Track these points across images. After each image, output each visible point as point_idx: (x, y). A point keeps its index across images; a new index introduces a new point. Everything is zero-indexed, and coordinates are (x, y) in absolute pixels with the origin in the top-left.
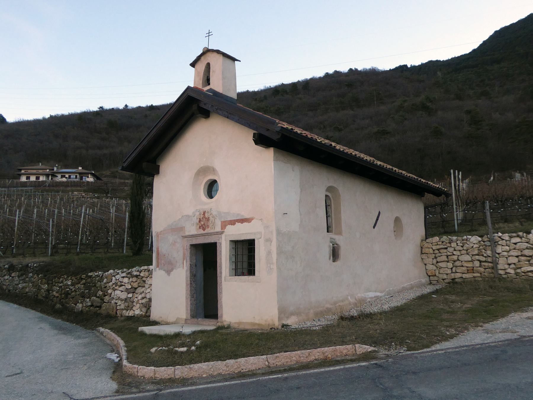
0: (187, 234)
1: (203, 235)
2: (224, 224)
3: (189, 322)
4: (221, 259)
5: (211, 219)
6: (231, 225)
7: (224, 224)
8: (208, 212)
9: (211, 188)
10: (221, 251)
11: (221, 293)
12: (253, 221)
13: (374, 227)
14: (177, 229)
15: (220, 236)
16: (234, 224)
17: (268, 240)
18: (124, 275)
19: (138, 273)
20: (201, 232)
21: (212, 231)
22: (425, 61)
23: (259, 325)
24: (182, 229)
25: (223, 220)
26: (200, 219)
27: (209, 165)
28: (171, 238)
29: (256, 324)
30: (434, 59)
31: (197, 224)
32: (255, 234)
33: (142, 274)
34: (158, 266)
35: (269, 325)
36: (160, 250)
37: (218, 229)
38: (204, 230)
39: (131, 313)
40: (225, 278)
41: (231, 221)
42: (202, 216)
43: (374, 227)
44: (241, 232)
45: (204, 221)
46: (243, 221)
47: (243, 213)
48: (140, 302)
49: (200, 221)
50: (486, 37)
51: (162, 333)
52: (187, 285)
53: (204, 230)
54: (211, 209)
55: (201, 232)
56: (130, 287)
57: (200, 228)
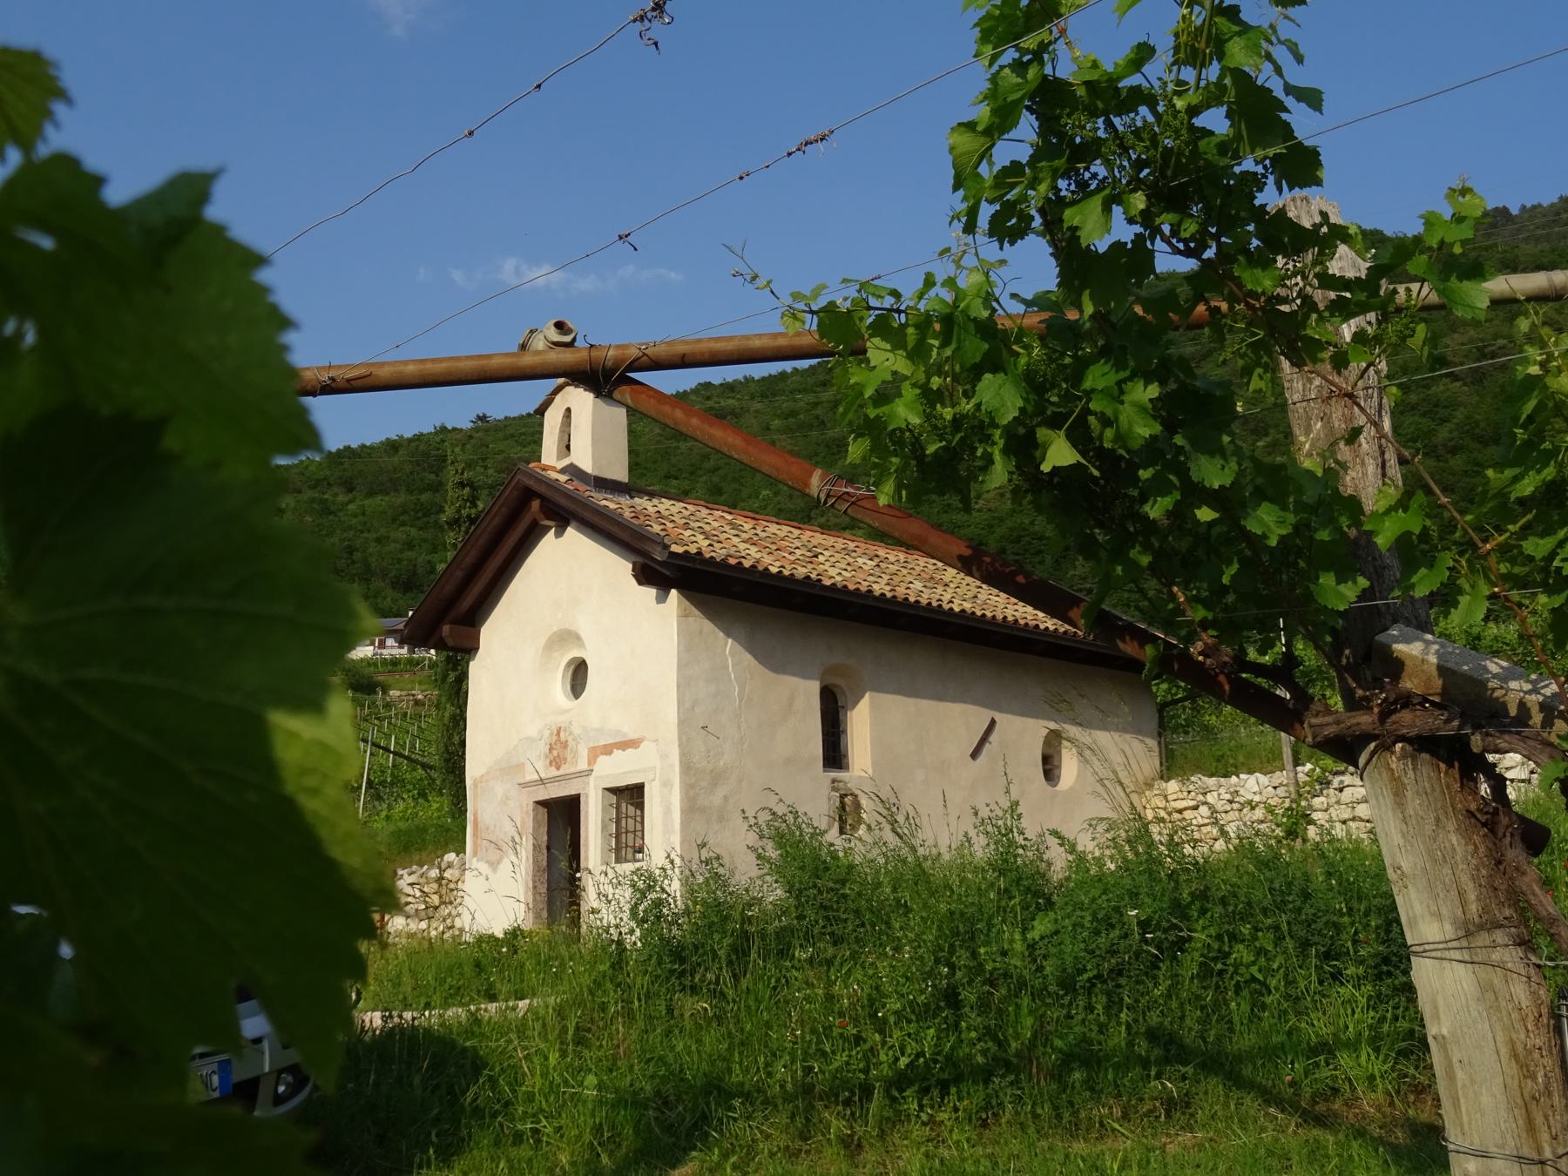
5: (571, 743)
9: (578, 674)
13: (975, 755)
16: (610, 753)
17: (666, 784)
20: (554, 772)
34: (475, 854)
37: (582, 765)
41: (605, 746)
43: (975, 755)
44: (620, 769)
47: (625, 729)
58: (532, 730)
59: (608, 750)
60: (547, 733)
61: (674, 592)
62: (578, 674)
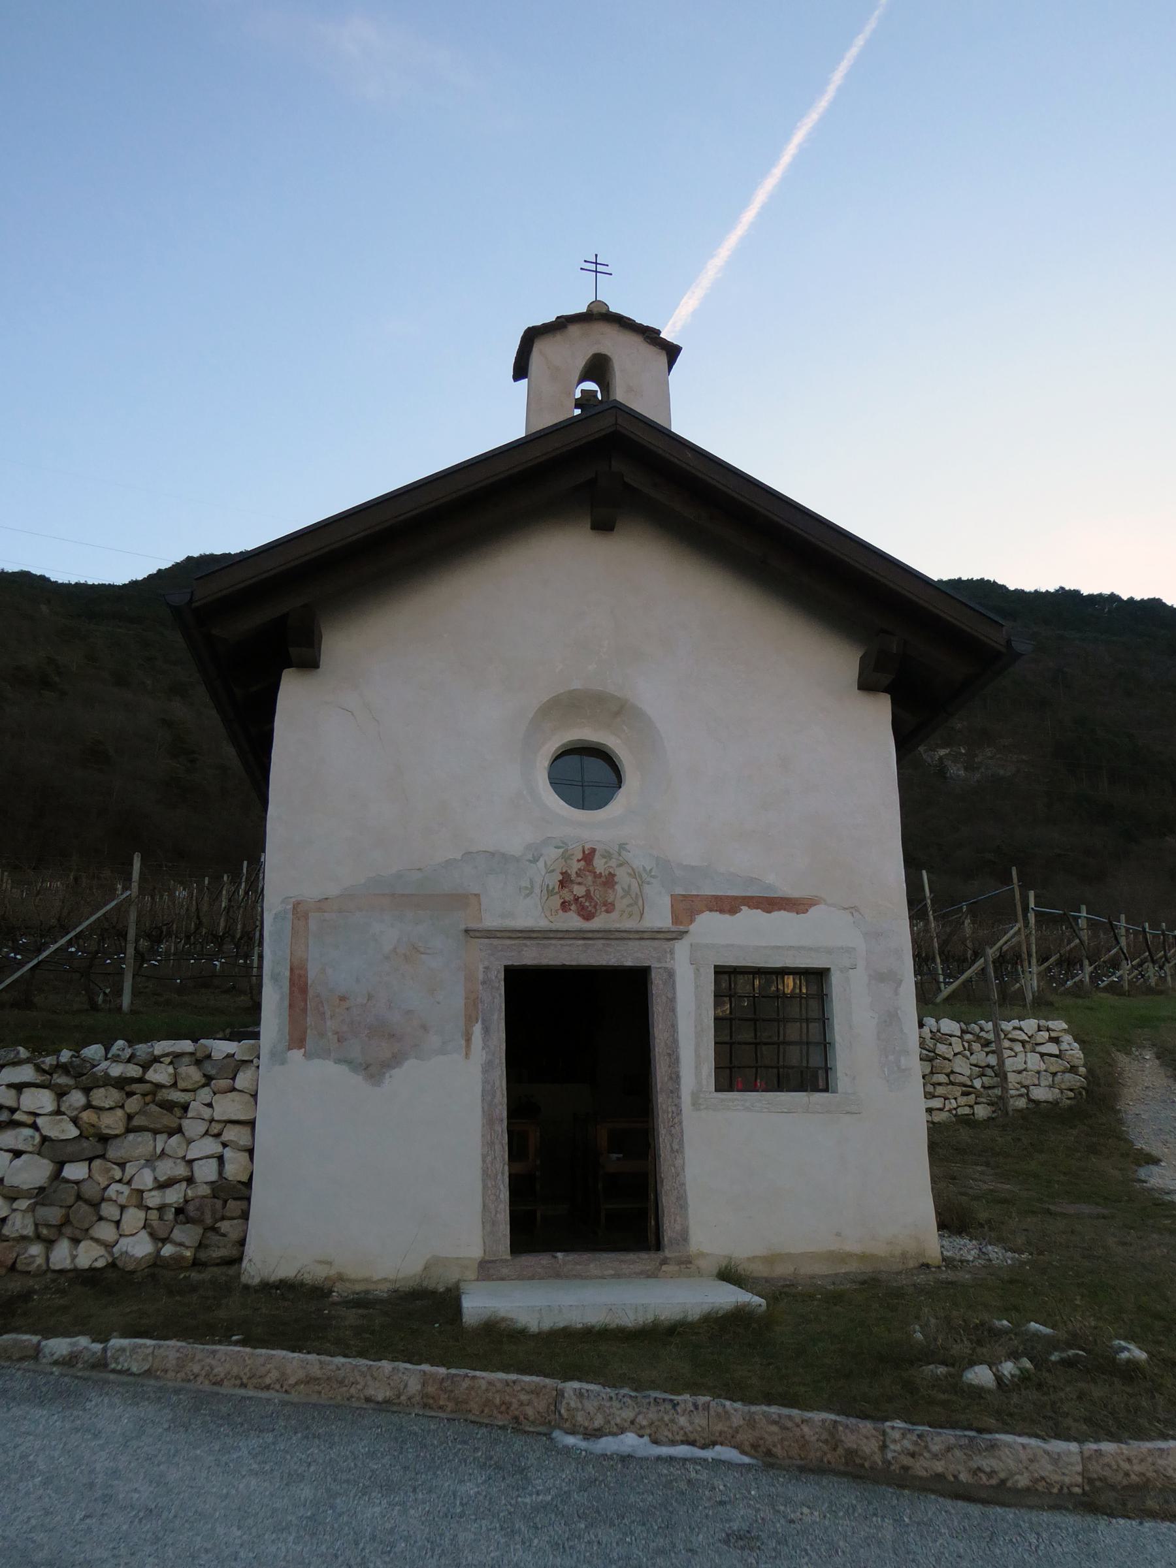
0: (490, 922)
1: (581, 935)
3: (505, 1271)
4: (673, 1027)
5: (622, 875)
6: (721, 911)
7: (687, 908)
8: (607, 855)
9: (588, 772)
12: (812, 910)
15: (667, 945)
16: (733, 911)
17: (883, 977)
18: (26, 1073)
19: (134, 1071)
20: (573, 921)
21: (629, 924)
22: (976, 577)
23: (863, 1257)
24: (461, 900)
25: (680, 891)
26: (565, 874)
29: (850, 1255)
30: (1000, 582)
31: (551, 893)
32: (829, 951)
33: (151, 1075)
34: (297, 1039)
35: (904, 1255)
36: (312, 975)
37: (659, 917)
39: (88, 1256)
40: (695, 1097)
41: (716, 898)
42: (575, 866)
45: (585, 883)
46: (770, 904)
47: (771, 879)
48: (153, 1199)
49: (562, 884)
50: (166, 565)
51: (629, 1319)
52: (489, 1121)
53: (588, 917)
54: (622, 846)
55: (573, 921)
56: (73, 1132)
57: (565, 906)
58: (515, 841)
59: (728, 905)
60: (552, 853)
62: (588, 772)
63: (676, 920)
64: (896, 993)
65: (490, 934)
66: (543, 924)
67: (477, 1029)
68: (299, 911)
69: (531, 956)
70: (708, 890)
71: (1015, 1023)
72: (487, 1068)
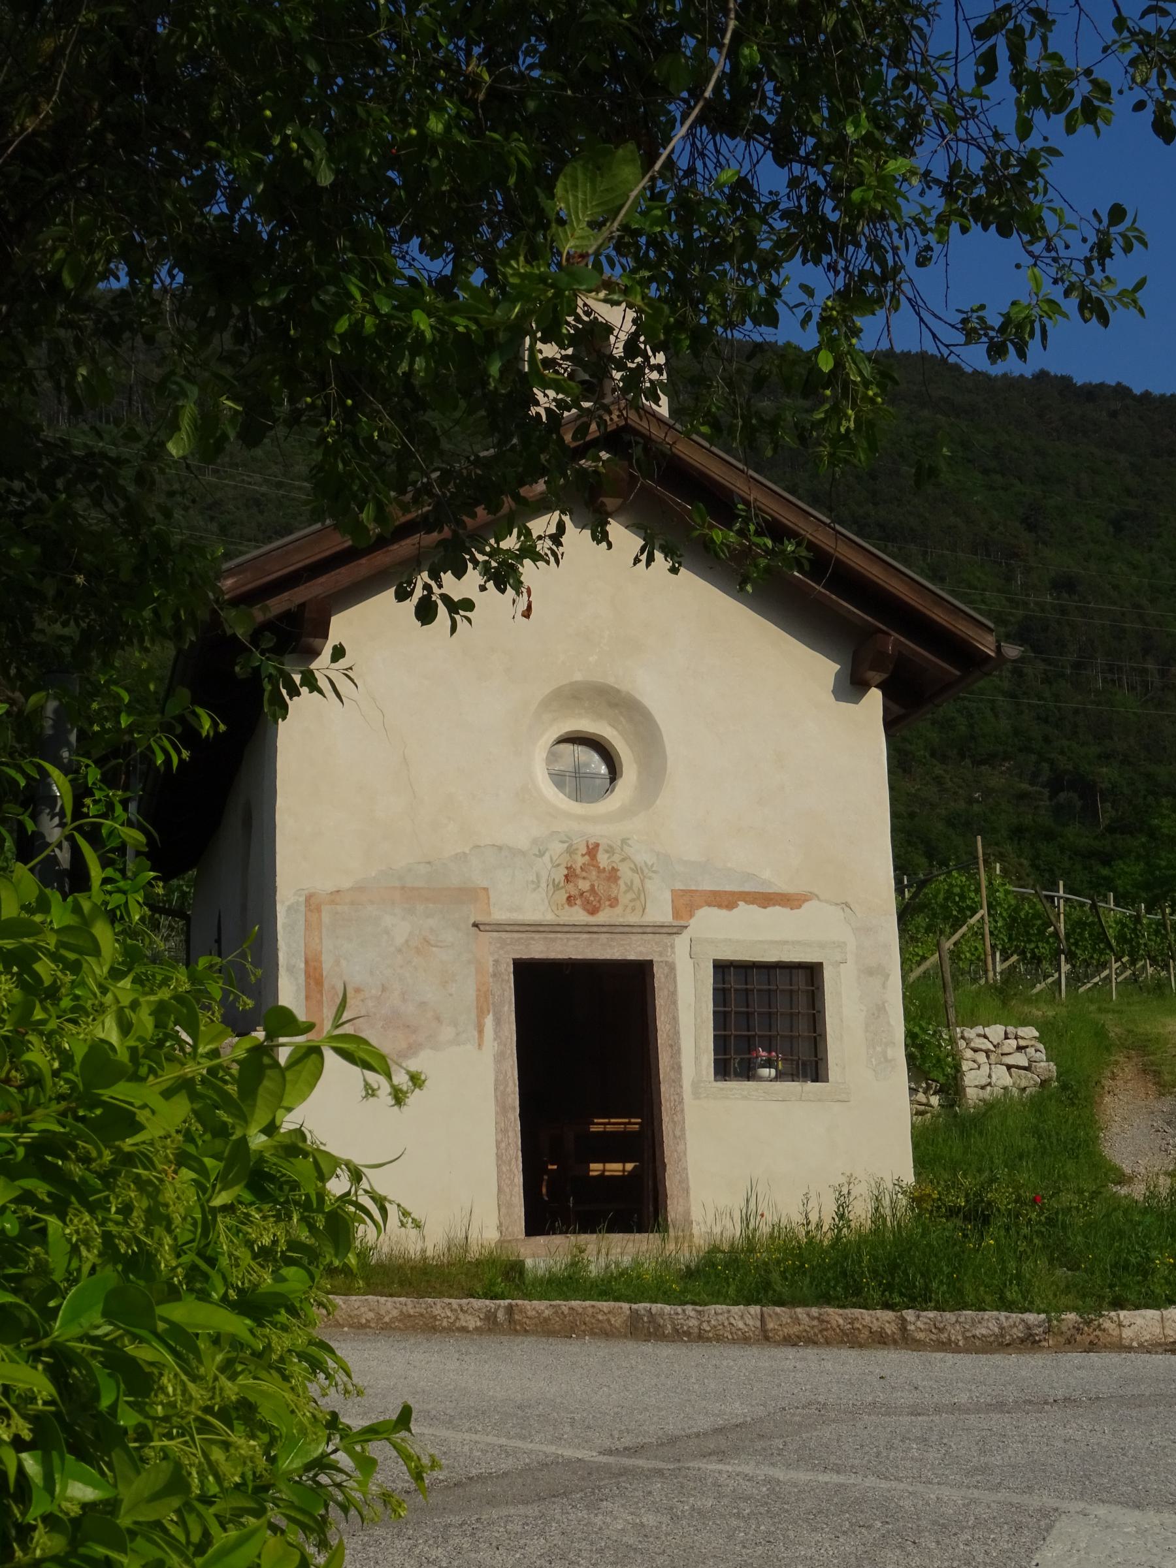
0: (499, 915)
2: (687, 902)
4: (675, 1020)
5: (625, 871)
8: (610, 850)
10: (673, 993)
11: (682, 1137)
12: (806, 905)
14: (441, 893)
15: (666, 939)
20: (578, 915)
21: (633, 919)
25: (679, 886)
27: (611, 681)
28: (400, 927)
31: (557, 887)
37: (660, 911)
38: (593, 911)
40: (696, 1085)
42: (580, 861)
45: (589, 877)
46: (765, 899)
47: (766, 874)
52: (502, 1109)
53: (593, 911)
55: (578, 915)
57: (570, 900)
59: (726, 900)
60: (557, 848)
61: (875, 696)
63: (676, 914)
64: (884, 986)
65: (499, 927)
66: (549, 917)
67: (489, 1021)
68: (312, 903)
69: (539, 949)
70: (708, 886)
71: (980, 1029)
72: (499, 1058)
